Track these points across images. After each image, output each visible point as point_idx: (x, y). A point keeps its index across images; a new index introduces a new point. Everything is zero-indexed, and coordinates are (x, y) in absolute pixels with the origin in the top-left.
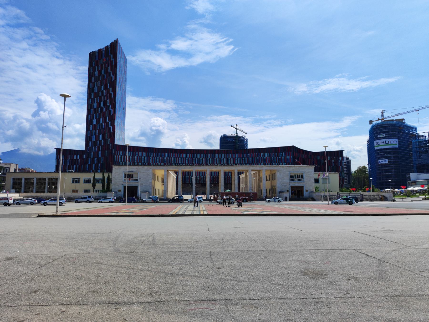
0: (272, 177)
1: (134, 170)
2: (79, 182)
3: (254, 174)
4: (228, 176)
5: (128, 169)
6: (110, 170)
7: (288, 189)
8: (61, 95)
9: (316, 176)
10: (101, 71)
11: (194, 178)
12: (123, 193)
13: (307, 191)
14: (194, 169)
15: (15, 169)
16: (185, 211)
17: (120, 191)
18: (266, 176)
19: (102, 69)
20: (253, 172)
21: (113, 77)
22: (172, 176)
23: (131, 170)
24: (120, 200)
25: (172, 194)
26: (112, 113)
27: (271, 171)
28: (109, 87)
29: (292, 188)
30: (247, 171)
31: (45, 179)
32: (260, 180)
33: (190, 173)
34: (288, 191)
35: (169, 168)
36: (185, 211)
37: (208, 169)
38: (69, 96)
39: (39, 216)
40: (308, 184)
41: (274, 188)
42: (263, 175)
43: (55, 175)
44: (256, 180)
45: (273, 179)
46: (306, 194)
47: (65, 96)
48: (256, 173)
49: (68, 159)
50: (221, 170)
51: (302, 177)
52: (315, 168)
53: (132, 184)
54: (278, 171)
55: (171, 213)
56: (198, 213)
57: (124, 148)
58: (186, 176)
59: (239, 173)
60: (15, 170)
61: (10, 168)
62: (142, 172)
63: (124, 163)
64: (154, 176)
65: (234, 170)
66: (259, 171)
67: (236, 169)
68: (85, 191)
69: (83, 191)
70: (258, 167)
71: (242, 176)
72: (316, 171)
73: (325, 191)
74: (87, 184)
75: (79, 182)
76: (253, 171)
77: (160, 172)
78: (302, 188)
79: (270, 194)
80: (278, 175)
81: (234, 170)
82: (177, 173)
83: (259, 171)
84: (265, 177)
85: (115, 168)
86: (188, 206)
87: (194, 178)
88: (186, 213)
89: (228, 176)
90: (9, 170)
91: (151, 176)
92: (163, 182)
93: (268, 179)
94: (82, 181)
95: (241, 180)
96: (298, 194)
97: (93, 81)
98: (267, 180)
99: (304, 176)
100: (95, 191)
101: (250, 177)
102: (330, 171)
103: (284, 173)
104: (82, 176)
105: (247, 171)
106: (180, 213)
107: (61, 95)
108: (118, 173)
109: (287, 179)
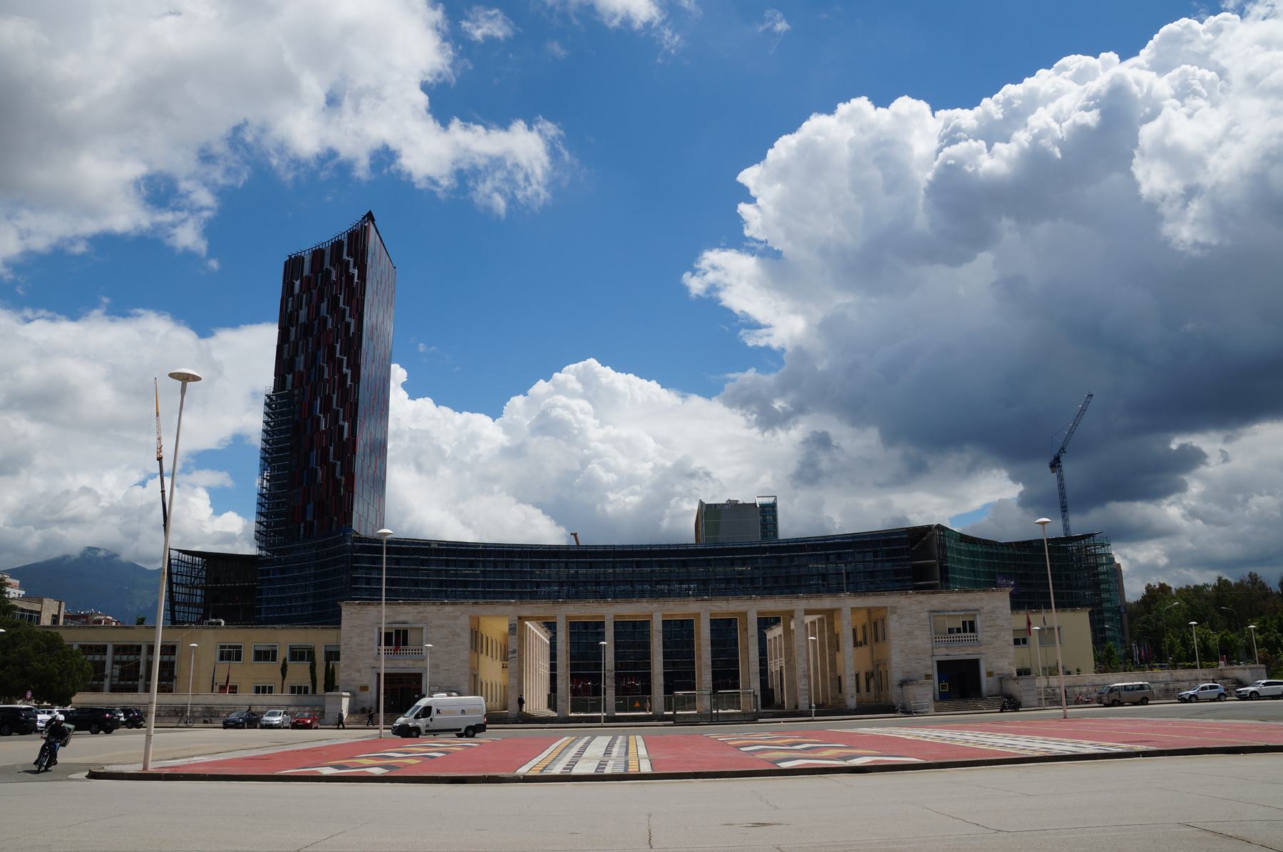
0: (873, 632)
1: (408, 618)
2: (238, 658)
3: (813, 623)
4: (725, 631)
5: (383, 615)
6: (333, 620)
7: (930, 672)
8: (172, 375)
9: (1020, 620)
10: (318, 308)
11: (608, 643)
12: (375, 696)
13: (990, 674)
14: (609, 612)
15: (54, 616)
16: (572, 764)
17: (364, 688)
18: (854, 631)
19: (321, 300)
20: (808, 619)
21: (353, 322)
22: (537, 634)
23: (399, 619)
24: (365, 715)
25: (536, 703)
26: (346, 435)
27: (869, 610)
28: (338, 355)
29: (943, 666)
30: (790, 614)
31: (139, 648)
32: (835, 645)
33: (595, 628)
34: (928, 677)
35: (527, 609)
36: (572, 764)
37: (656, 612)
38: (196, 379)
39: (93, 776)
40: (997, 658)
41: (881, 669)
42: (845, 627)
43: (177, 636)
44: (822, 644)
45: (877, 640)
46: (986, 683)
47: (185, 378)
48: (821, 620)
49: (215, 587)
50: (703, 612)
51: (973, 629)
52: (1012, 595)
53: (404, 664)
54: (894, 610)
55: (523, 771)
56: (620, 770)
57: (373, 547)
58: (585, 634)
59: (765, 622)
60: (55, 619)
61: (39, 613)
62: (439, 625)
63: (371, 596)
64: (477, 641)
65: (744, 614)
66: (830, 614)
67: (751, 608)
68: (257, 690)
69: (253, 689)
70: (827, 602)
71: (775, 633)
72: (1017, 605)
73: (1051, 671)
74: (264, 665)
75: (238, 658)
76: (808, 612)
77: (496, 624)
78: (975, 664)
79: (868, 690)
80: (893, 625)
81: (744, 614)
82: (551, 626)
83: (830, 614)
84: (851, 633)
85: (349, 612)
86: (588, 743)
87: (608, 643)
88: (577, 771)
89: (725, 631)
90: (39, 619)
91: (466, 638)
92: (505, 658)
93: (860, 638)
94: (247, 654)
95: (770, 647)
96: (961, 685)
97: (292, 338)
98: (856, 644)
99: (978, 624)
100: (287, 688)
101: (797, 634)
102: (1061, 606)
103: (914, 626)
104: (251, 638)
105: (790, 614)
106: (557, 770)
107: (172, 375)
108: (362, 627)
109: (923, 640)
